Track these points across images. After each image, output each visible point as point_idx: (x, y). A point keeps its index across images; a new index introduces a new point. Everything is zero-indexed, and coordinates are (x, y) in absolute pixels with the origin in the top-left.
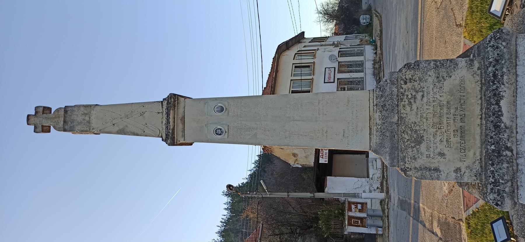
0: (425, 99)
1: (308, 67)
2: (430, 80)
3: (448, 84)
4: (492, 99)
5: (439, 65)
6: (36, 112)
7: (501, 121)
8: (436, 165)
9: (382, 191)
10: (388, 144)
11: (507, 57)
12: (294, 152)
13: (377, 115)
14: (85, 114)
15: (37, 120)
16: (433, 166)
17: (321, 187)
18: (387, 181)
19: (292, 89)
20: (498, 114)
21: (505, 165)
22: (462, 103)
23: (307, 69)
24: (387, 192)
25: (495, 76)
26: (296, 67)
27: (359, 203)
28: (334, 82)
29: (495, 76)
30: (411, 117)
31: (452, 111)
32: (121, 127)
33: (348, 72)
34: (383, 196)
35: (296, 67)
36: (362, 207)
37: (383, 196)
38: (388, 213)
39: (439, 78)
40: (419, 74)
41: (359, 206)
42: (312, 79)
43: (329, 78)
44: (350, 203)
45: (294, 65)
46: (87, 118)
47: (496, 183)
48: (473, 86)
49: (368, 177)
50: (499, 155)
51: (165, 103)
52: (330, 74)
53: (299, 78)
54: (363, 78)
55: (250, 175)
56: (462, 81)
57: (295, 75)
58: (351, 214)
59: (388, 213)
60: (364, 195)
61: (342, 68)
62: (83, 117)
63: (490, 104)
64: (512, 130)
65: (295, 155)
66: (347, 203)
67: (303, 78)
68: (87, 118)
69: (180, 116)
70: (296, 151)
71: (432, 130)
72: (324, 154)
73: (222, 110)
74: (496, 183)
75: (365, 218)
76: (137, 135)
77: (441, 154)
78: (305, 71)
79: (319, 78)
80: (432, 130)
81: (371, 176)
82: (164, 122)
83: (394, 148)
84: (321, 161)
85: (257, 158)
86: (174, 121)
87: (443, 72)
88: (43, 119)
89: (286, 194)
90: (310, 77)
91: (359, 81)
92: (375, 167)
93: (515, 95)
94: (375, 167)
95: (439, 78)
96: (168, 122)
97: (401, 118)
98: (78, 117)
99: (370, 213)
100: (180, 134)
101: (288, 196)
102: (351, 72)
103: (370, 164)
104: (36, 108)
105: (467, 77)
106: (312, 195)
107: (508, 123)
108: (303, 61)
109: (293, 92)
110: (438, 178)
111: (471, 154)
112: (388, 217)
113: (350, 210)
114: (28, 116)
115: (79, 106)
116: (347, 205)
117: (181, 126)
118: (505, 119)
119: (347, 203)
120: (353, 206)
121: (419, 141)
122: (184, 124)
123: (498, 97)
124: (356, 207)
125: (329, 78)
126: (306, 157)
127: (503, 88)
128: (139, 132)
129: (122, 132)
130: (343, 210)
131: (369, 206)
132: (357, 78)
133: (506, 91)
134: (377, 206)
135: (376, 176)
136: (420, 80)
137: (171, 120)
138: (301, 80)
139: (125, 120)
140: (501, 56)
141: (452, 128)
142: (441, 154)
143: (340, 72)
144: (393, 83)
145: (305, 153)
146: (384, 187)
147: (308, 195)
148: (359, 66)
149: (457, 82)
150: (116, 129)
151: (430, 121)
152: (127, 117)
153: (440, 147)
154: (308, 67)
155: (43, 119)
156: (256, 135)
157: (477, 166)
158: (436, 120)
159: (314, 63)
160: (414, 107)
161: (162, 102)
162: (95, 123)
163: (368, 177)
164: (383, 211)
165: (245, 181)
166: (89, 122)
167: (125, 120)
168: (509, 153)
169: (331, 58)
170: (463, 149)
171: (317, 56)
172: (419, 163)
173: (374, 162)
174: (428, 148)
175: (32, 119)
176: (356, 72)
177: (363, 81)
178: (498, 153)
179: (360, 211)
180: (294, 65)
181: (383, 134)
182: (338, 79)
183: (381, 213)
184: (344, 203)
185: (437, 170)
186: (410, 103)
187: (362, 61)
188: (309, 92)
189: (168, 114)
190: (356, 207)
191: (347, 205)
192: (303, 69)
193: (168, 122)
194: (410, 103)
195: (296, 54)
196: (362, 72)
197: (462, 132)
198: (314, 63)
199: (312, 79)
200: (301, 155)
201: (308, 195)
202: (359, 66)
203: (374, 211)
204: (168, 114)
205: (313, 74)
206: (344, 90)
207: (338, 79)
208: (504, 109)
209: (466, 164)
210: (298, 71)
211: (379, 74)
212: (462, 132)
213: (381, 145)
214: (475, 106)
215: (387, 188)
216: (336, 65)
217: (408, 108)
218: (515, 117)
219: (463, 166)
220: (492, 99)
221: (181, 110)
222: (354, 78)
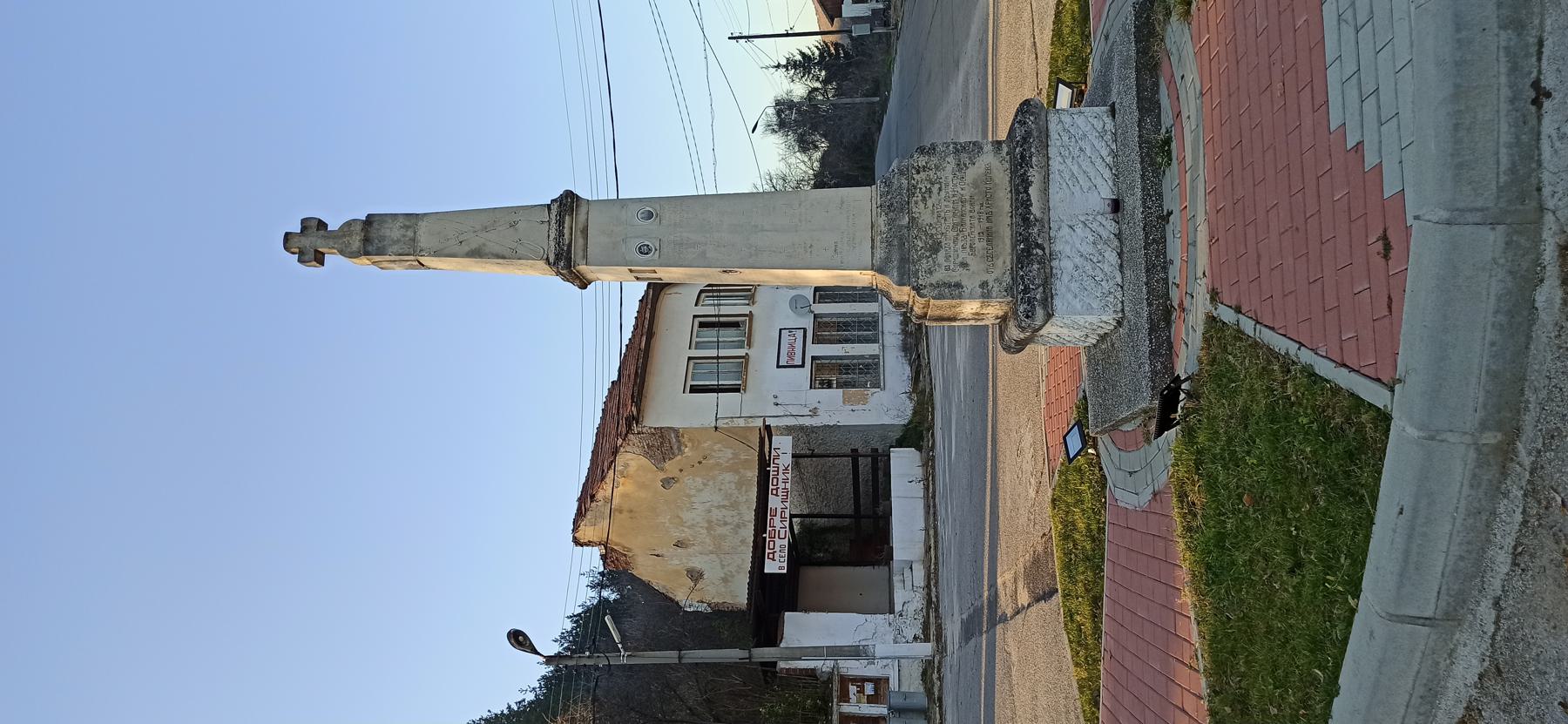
0: (943, 194)
1: (736, 325)
2: (949, 168)
3: (972, 173)
4: (1020, 185)
5: (959, 149)
6: (304, 228)
7: (1030, 213)
8: (957, 279)
9: (927, 640)
10: (895, 257)
11: (1035, 134)
12: (691, 565)
13: (882, 220)
14: (407, 227)
15: (306, 242)
16: (953, 281)
17: (770, 634)
18: (937, 610)
19: (690, 382)
20: (1027, 204)
21: (1036, 266)
22: (988, 197)
23: (732, 331)
24: (939, 637)
25: (1023, 157)
26: (702, 325)
27: (869, 680)
28: (803, 366)
29: (1023, 157)
30: (925, 216)
31: (977, 208)
32: (474, 246)
33: (840, 342)
34: (926, 649)
35: (702, 325)
36: (876, 689)
37: (926, 649)
38: (941, 689)
39: (960, 167)
40: (935, 160)
41: (869, 689)
42: (746, 357)
43: (791, 355)
44: (845, 681)
45: (697, 320)
46: (410, 234)
47: (1026, 290)
48: (1002, 177)
49: (892, 611)
50: (1030, 254)
51: (555, 207)
52: (792, 346)
53: (713, 353)
54: (877, 357)
55: (544, 677)
56: (988, 169)
57: (699, 346)
58: (846, 708)
59: (941, 689)
60: (880, 650)
61: (824, 330)
62: (403, 231)
63: (1018, 192)
64: (1045, 224)
65: (695, 576)
66: (836, 678)
67: (723, 353)
68: (410, 234)
69: (580, 226)
70: (697, 563)
71: (952, 234)
72: (777, 549)
73: (650, 215)
74: (1026, 290)
75: (884, 718)
76: (504, 257)
77: (964, 265)
78: (729, 335)
79: (762, 354)
80: (952, 234)
81: (898, 608)
82: (553, 236)
83: (904, 261)
84: (771, 567)
85: (569, 626)
86: (566, 236)
87: (964, 157)
88: (310, 241)
89: (674, 653)
90: (741, 352)
91: (867, 366)
92: (908, 584)
93: (1046, 180)
94: (908, 584)
95: (960, 167)
96: (561, 234)
97: (912, 219)
98: (393, 232)
99: (896, 701)
100: (580, 253)
101: (680, 658)
102: (847, 341)
103: (896, 578)
104: (303, 221)
105: (993, 165)
106: (745, 654)
107: (1038, 215)
108: (724, 310)
109: (694, 389)
110: (960, 297)
111: (1000, 262)
112: (940, 699)
113: (844, 697)
114: (287, 234)
115: (395, 216)
116: (836, 686)
117: (581, 241)
118: (1035, 210)
119: (836, 678)
120: (853, 689)
121: (935, 248)
122: (586, 238)
123: (1026, 183)
124: (861, 691)
125: (791, 355)
126: (725, 580)
127: (1031, 172)
128: (507, 252)
129: (476, 254)
130: (827, 699)
131: (894, 684)
132: (862, 357)
133: (1035, 175)
134: (914, 685)
135: (911, 608)
136: (937, 167)
137: (566, 231)
138: (718, 358)
139: (482, 236)
140: (1029, 134)
141: (977, 230)
142: (964, 265)
143: (818, 340)
144: (901, 173)
145: (723, 566)
146: (931, 629)
147: (733, 654)
148: (867, 328)
149: (982, 170)
150: (466, 249)
151: (950, 222)
152: (485, 229)
153: (963, 255)
154: (736, 325)
155: (310, 241)
156: (704, 253)
157: (1008, 279)
158: (957, 220)
159: (750, 315)
160: (930, 203)
161: (549, 206)
162: (424, 240)
163: (892, 611)
164: (929, 692)
165: (530, 697)
166: (414, 240)
167: (482, 236)
168: (1040, 252)
169: (796, 303)
170: (990, 257)
171: (758, 297)
172: (934, 279)
173: (907, 573)
174: (947, 258)
175: (294, 242)
176: (860, 342)
177: (877, 364)
178: (1027, 252)
179: (872, 700)
180: (697, 320)
181: (890, 244)
182: (813, 358)
183: (924, 702)
184: (830, 680)
185: (958, 285)
186: (924, 199)
187: (873, 315)
188: (738, 390)
189: (561, 223)
190: (861, 691)
191: (836, 686)
192: (723, 331)
193: (561, 234)
194: (924, 199)
195: (702, 291)
196: (875, 341)
197: (989, 235)
198: (750, 315)
199: (746, 357)
200: (712, 572)
201: (733, 654)
202: (867, 328)
203: (906, 695)
204: (561, 223)
205: (749, 345)
206: (830, 386)
207: (813, 358)
208: (1034, 198)
209: (994, 276)
210: (710, 335)
211: (916, 346)
212: (989, 235)
213: (888, 260)
214: (1004, 202)
215: (939, 628)
216: (808, 323)
217: (922, 205)
218: (1046, 209)
219: (990, 278)
220: (1020, 185)
221: (582, 217)
222: (853, 357)
